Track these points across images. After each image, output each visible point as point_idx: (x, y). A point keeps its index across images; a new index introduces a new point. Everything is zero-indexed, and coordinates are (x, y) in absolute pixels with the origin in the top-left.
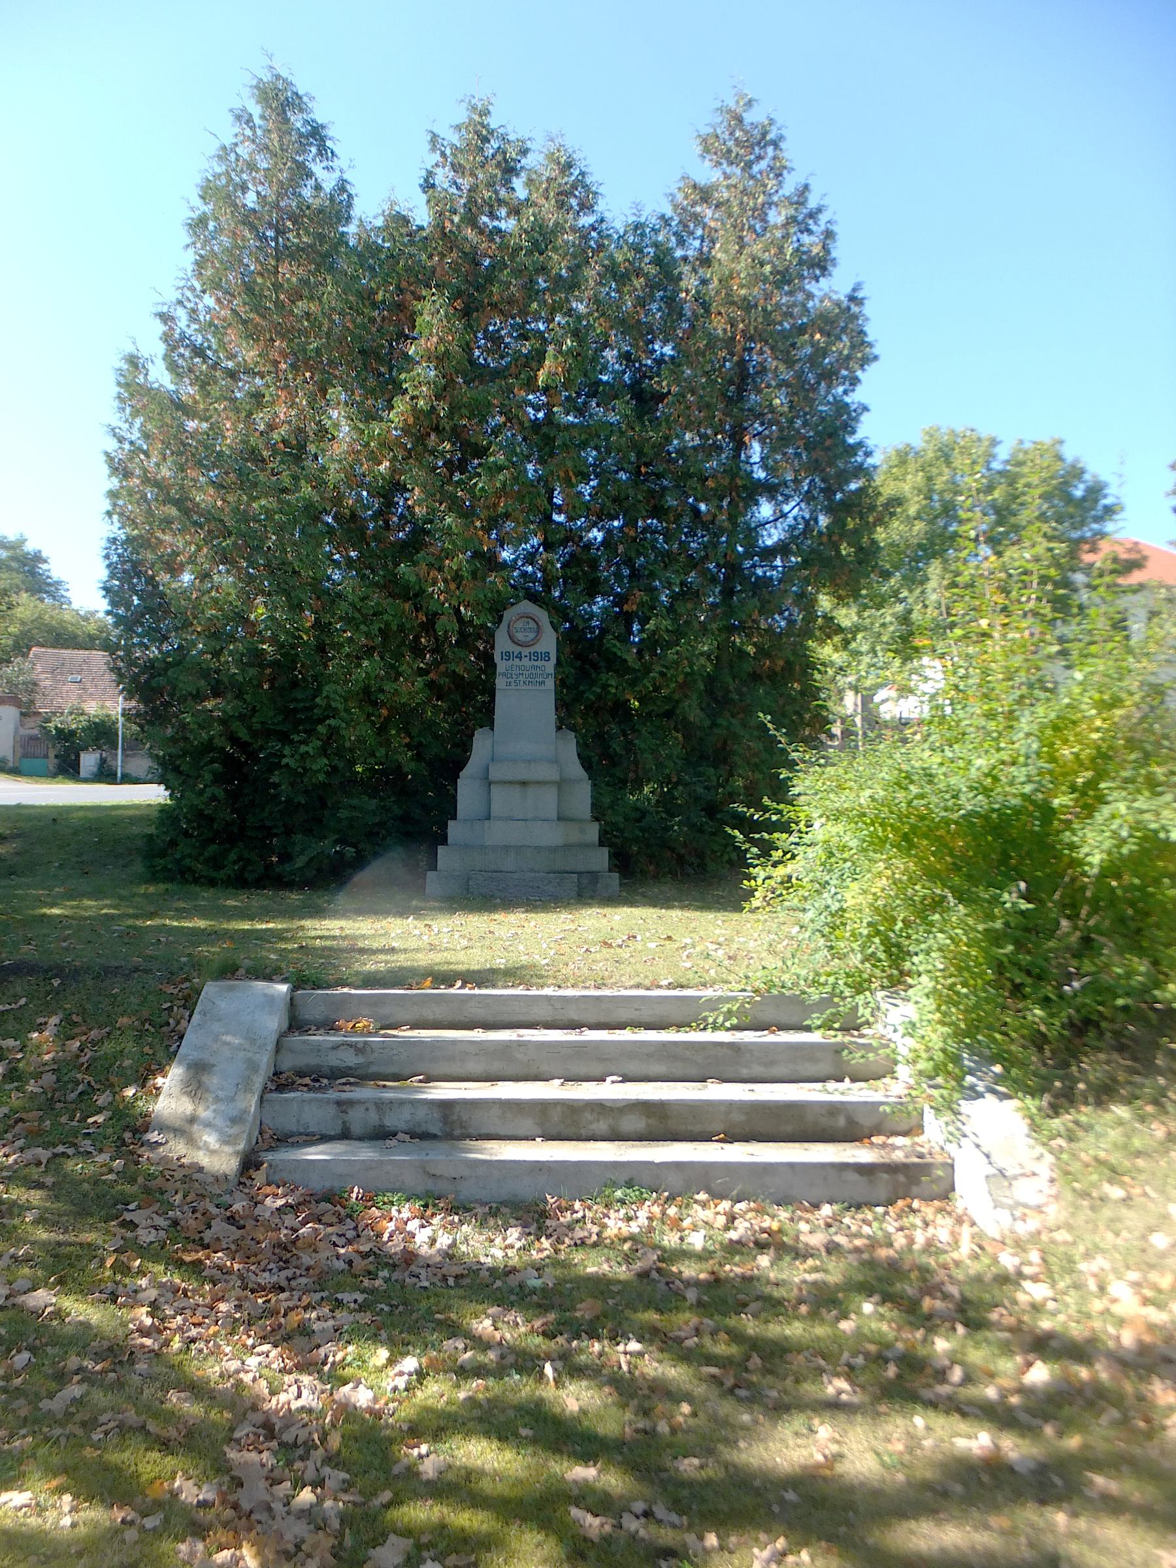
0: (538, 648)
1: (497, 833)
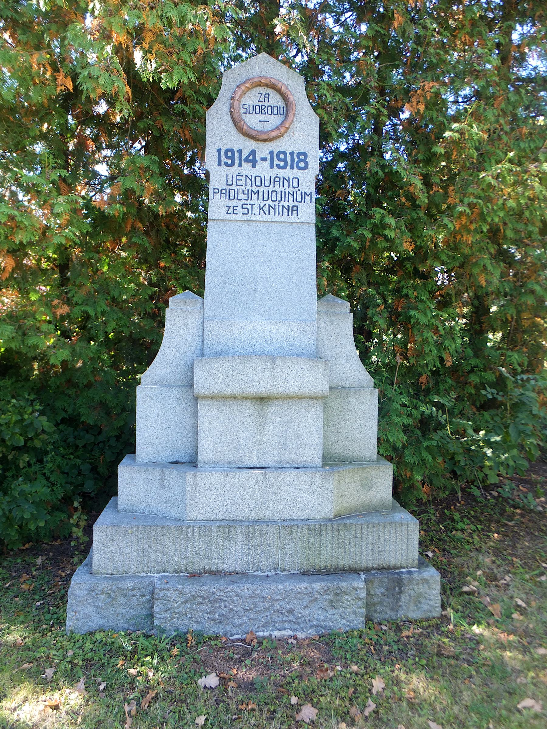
0: (285, 144)
1: (210, 496)
